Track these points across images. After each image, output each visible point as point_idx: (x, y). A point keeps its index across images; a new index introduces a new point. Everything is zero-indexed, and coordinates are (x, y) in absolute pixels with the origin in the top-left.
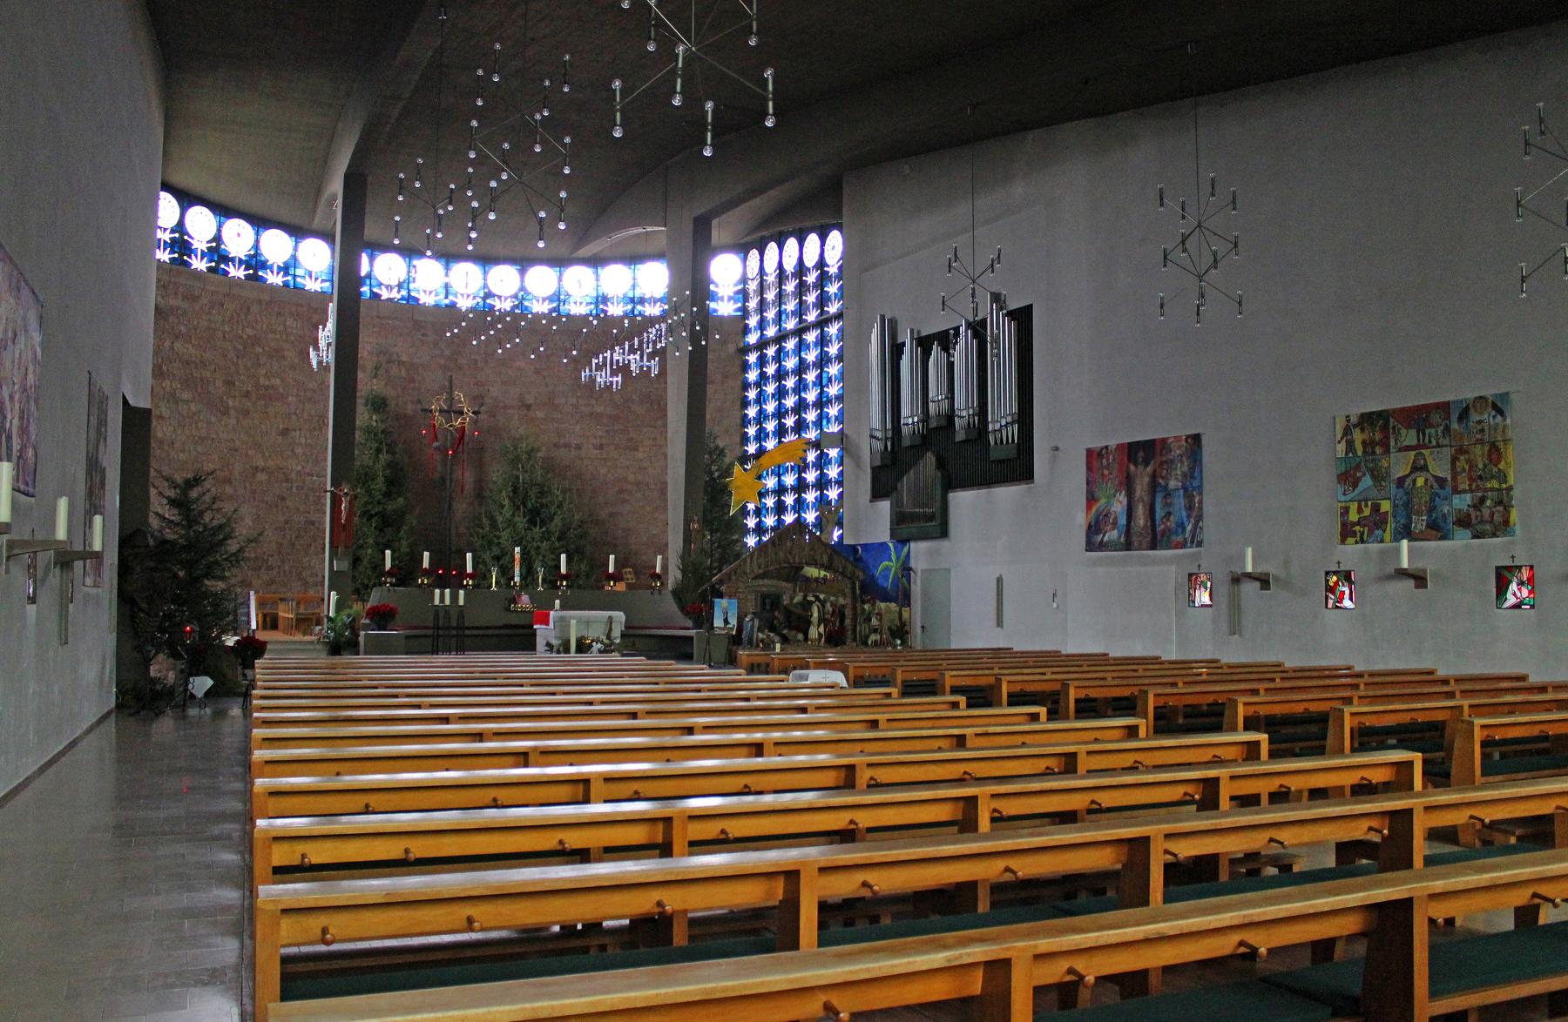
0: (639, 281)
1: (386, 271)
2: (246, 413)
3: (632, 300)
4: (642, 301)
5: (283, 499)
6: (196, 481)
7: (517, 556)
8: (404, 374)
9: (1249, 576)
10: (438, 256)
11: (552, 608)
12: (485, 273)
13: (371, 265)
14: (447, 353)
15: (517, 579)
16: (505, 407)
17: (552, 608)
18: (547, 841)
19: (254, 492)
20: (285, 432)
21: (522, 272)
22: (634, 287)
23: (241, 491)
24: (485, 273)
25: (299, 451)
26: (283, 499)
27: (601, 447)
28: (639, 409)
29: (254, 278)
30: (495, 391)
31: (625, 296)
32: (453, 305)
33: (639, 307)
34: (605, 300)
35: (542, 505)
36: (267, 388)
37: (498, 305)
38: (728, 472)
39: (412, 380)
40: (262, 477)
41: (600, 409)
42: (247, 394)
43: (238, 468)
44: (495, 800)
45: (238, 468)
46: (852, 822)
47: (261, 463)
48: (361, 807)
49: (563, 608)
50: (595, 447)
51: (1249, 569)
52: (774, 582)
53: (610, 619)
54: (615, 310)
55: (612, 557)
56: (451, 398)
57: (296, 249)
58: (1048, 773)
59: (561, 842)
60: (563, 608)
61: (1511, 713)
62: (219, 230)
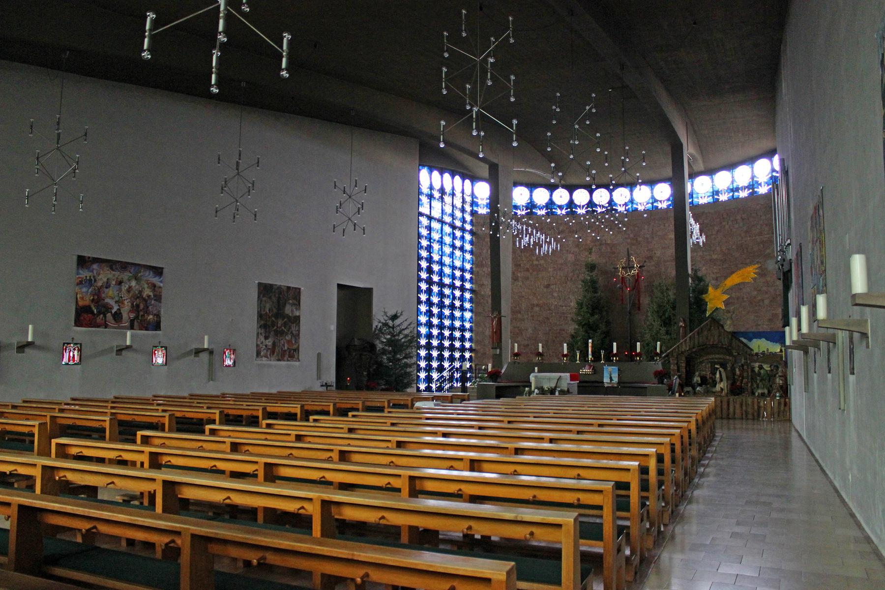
0: (736, 178)
1: (701, 189)
2: (527, 278)
3: (732, 190)
4: (737, 189)
5: (548, 319)
6: (394, 317)
7: (590, 345)
8: (609, 250)
9: (204, 350)
10: (644, 183)
11: (533, 371)
12: (652, 190)
13: (692, 186)
14: (632, 236)
15: (590, 357)
16: (665, 261)
17: (533, 371)
18: (452, 488)
19: (533, 316)
20: (548, 286)
21: (631, 191)
22: (733, 182)
23: (526, 316)
24: (652, 190)
25: (555, 294)
26: (548, 319)
27: (717, 279)
28: (737, 255)
29: (754, 193)
30: (658, 253)
31: (728, 188)
32: (636, 209)
33: (736, 194)
34: (717, 193)
35: (674, 315)
36: (537, 265)
37: (660, 206)
38: (704, 291)
39: (614, 253)
40: (537, 309)
41: (715, 257)
42: (528, 270)
43: (524, 306)
44: (579, 475)
45: (524, 306)
46: (460, 490)
47: (535, 302)
48: (446, 466)
49: (539, 371)
50: (713, 279)
51: (206, 346)
52: (722, 356)
53: (559, 379)
54: (723, 198)
55: (615, 344)
56: (629, 260)
57: (551, 196)
58: (329, 460)
59: (579, 500)
60: (539, 371)
61: (27, 419)
62: (531, 196)
